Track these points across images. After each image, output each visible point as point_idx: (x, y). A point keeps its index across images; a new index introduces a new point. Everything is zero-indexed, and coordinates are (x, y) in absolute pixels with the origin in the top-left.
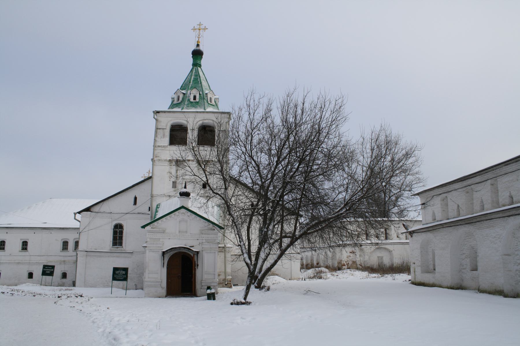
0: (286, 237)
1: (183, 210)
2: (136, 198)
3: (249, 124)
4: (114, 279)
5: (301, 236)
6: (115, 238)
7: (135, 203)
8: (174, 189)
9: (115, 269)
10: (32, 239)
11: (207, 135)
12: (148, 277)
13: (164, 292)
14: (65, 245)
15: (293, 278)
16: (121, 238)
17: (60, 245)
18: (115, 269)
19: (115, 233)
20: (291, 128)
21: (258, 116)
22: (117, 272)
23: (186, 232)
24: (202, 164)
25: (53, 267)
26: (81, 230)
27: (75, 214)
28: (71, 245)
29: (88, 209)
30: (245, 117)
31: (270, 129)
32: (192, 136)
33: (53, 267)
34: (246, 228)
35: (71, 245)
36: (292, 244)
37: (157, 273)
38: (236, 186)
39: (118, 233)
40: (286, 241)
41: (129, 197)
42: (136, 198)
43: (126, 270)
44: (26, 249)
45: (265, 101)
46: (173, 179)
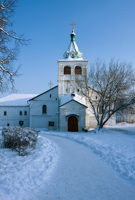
0: (111, 111)
1: (73, 101)
2: (51, 95)
3: (97, 70)
4: (49, 125)
5: (116, 111)
6: (43, 111)
7: (51, 97)
8: (67, 92)
9: (50, 122)
10: (8, 111)
11: (78, 70)
12: (61, 125)
13: (67, 130)
14: (21, 113)
15: (57, 112)
16: (46, 110)
17: (19, 113)
18: (50, 122)
19: (43, 108)
20: (113, 73)
21: (100, 68)
22: (50, 123)
23: (74, 109)
24: (77, 81)
25: (23, 122)
26: (30, 106)
27: (28, 101)
28: (23, 113)
29: (32, 99)
30: (96, 68)
31: (104, 72)
32: (73, 70)
33: (23, 122)
34: (97, 108)
35: (23, 113)
36: (113, 113)
37: (64, 123)
38: (130, 121)
39: (44, 108)
40: (111, 112)
41: (48, 94)
42: (51, 95)
43: (53, 122)
44: (26, 114)
45: (103, 61)
46: (66, 88)
